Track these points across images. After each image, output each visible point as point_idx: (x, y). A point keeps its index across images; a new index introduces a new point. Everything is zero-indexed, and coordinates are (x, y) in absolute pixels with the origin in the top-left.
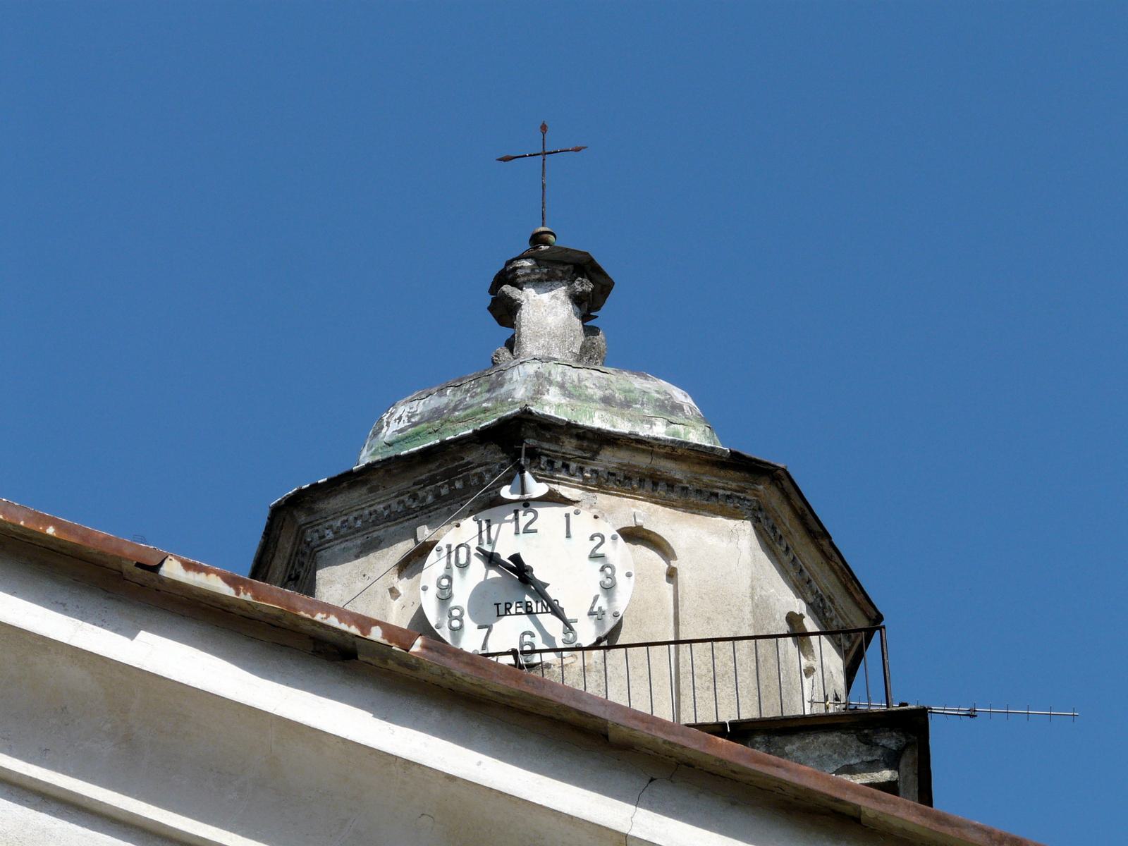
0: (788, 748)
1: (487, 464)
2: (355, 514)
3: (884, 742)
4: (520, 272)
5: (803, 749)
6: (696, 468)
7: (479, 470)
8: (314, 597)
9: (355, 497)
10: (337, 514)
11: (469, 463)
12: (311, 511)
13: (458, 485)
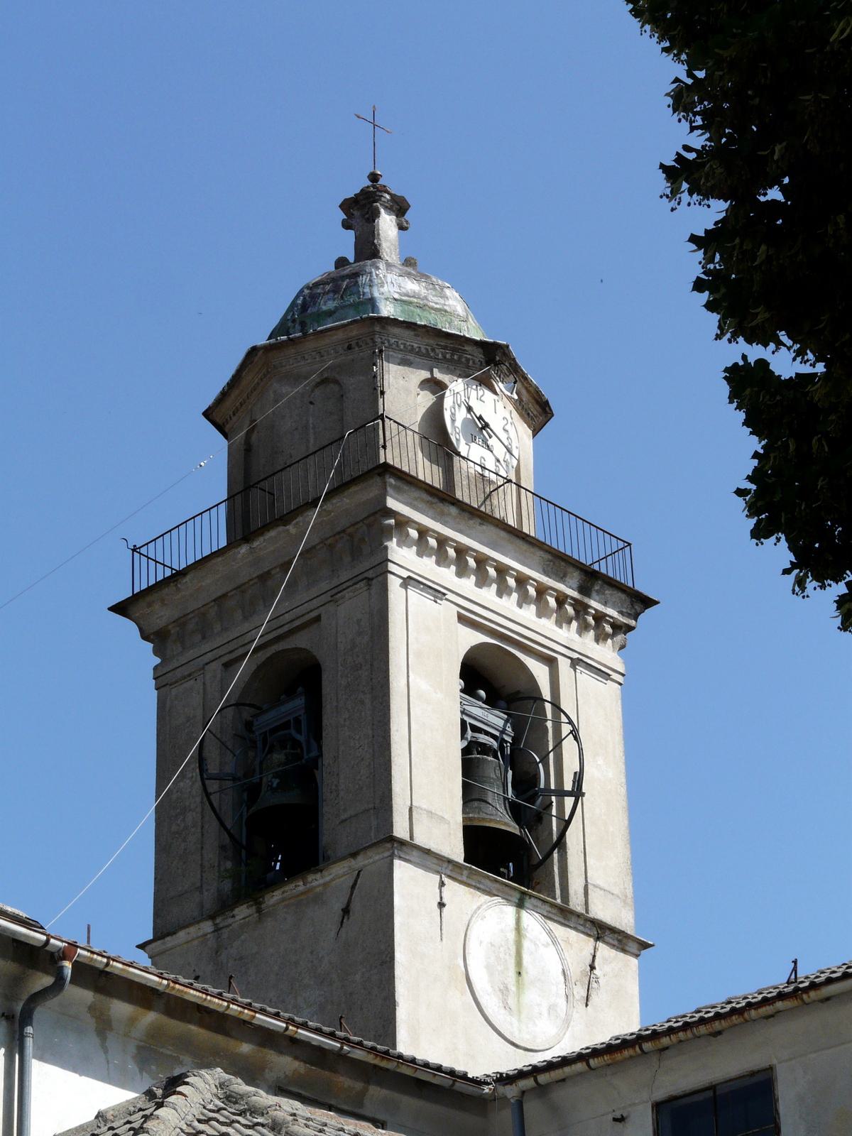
0: (607, 592)
1: (473, 356)
2: (403, 341)
3: (636, 607)
4: (383, 199)
5: (611, 595)
6: (530, 398)
7: (469, 356)
8: (845, 583)
9: (407, 333)
10: (395, 336)
11: (465, 350)
12: (383, 328)
13: (456, 357)
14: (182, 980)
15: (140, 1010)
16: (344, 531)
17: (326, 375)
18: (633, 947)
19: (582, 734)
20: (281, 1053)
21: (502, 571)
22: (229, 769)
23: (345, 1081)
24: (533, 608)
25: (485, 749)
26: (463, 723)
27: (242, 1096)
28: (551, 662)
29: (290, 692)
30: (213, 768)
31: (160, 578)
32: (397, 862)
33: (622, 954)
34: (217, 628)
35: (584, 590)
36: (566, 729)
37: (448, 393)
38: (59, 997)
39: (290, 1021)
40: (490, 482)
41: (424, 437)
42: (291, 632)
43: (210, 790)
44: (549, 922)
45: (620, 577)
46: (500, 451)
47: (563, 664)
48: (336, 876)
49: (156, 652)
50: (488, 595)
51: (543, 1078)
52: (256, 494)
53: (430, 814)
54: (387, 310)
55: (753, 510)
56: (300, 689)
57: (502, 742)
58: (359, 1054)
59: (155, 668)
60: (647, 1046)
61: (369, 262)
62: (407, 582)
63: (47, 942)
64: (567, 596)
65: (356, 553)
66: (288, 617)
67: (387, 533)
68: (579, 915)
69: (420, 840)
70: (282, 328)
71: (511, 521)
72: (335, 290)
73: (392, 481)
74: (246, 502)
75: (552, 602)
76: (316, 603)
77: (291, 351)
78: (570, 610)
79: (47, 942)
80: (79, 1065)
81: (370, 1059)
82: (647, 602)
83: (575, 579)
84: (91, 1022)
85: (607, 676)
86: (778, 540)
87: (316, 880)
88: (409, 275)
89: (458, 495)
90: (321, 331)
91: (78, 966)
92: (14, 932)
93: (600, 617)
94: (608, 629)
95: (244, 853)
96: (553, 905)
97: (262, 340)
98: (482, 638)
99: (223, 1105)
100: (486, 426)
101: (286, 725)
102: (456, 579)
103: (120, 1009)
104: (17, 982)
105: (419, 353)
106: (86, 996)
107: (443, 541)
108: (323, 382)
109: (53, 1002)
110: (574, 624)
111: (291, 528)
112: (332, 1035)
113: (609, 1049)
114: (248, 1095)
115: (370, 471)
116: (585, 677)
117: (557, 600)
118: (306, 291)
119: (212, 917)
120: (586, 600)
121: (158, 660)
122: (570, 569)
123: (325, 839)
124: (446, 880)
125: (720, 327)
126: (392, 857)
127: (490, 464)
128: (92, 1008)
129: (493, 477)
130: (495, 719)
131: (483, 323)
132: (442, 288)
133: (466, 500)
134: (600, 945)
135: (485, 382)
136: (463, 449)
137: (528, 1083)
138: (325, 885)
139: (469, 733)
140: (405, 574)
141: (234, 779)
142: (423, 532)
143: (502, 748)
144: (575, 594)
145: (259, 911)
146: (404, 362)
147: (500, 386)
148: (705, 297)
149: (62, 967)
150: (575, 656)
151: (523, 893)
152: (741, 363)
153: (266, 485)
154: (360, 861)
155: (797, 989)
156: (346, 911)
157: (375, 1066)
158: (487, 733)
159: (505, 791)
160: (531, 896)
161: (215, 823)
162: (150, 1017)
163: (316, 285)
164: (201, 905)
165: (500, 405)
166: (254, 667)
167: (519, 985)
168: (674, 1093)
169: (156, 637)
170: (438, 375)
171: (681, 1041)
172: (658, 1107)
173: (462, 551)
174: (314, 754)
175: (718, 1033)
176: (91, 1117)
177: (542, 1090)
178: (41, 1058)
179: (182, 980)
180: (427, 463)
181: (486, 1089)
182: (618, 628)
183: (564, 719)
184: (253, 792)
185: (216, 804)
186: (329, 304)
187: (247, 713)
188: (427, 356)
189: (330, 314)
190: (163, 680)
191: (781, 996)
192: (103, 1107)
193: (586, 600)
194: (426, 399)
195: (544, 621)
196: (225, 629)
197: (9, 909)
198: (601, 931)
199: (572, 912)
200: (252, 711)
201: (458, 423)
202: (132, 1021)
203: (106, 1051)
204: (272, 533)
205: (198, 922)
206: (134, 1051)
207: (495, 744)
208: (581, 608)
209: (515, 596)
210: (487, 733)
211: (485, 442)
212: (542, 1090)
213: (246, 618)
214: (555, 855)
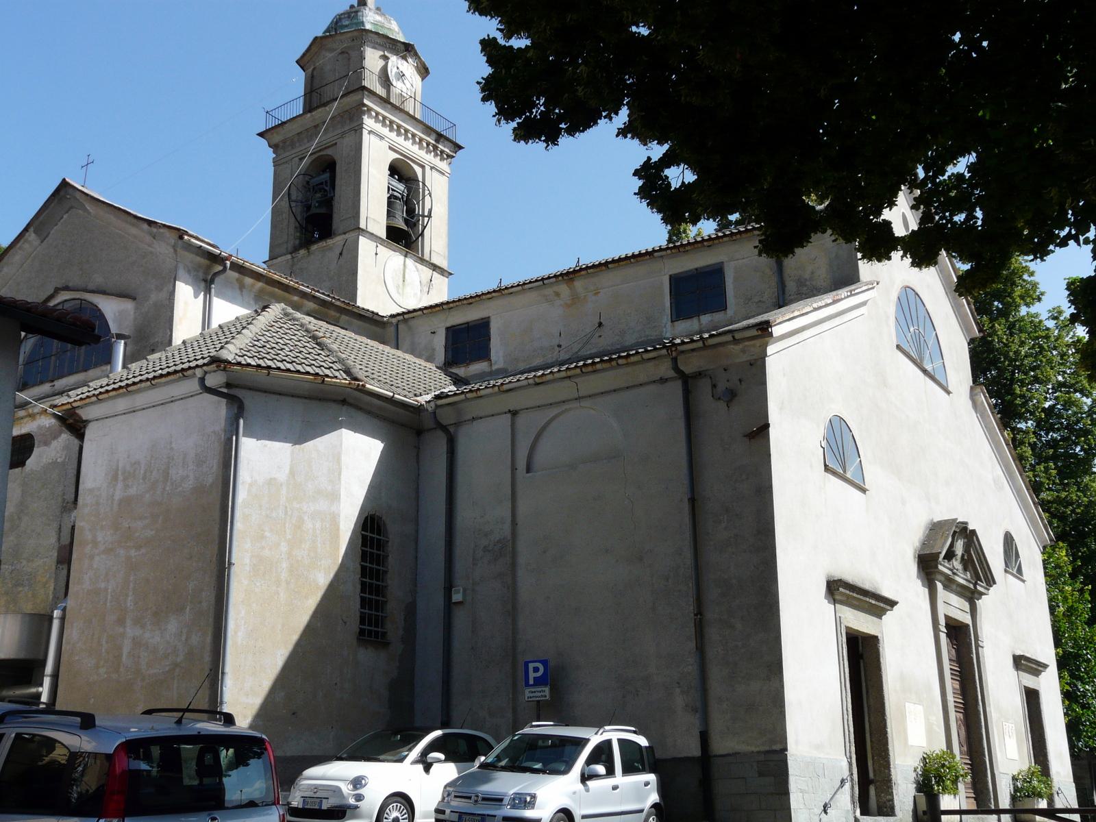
10: (370, 37)
14: (272, 271)
15: (255, 281)
16: (347, 111)
17: (343, 50)
18: (446, 274)
20: (309, 301)
21: (407, 131)
22: (299, 198)
23: (332, 313)
24: (417, 146)
25: (396, 198)
26: (389, 187)
27: (290, 314)
28: (423, 167)
29: (324, 171)
30: (294, 197)
31: (276, 124)
32: (360, 237)
33: (442, 277)
34: (297, 145)
35: (437, 141)
36: (427, 192)
37: (390, 61)
38: (224, 275)
39: (313, 289)
40: (404, 97)
41: (380, 77)
42: (326, 148)
43: (292, 206)
44: (416, 263)
45: (451, 137)
46: (409, 85)
47: (427, 168)
48: (337, 241)
49: (274, 152)
50: (401, 140)
51: (406, 316)
52: (314, 94)
53: (374, 220)
54: (368, 27)
55: (483, 90)
57: (403, 196)
58: (338, 303)
59: (274, 158)
60: (444, 307)
61: (362, 7)
62: (370, 132)
63: (393, 396)
64: (430, 143)
65: (351, 119)
66: (325, 142)
67: (363, 113)
68: (427, 261)
69: (369, 230)
70: (328, 30)
71: (411, 113)
72: (349, 17)
73: (366, 93)
74: (311, 96)
75: (425, 144)
76: (335, 138)
77: (331, 39)
78: (431, 148)
79: (393, 396)
80: (232, 300)
81: (342, 305)
82: (460, 148)
83: (434, 136)
84: (237, 285)
85: (443, 174)
86: (491, 103)
87: (330, 242)
88: (377, 14)
89: (391, 101)
90: (343, 33)
91: (232, 263)
92: (207, 249)
93: (442, 152)
94: (445, 156)
95: (304, 230)
96: (418, 257)
97: (320, 34)
98: (398, 156)
99: (300, 328)
100: (404, 75)
101: (322, 184)
102: (389, 133)
103: (248, 281)
104: (209, 268)
105: (380, 45)
106: (235, 275)
107: (385, 118)
108: (342, 53)
109: (222, 277)
110: (433, 153)
111: (327, 108)
112: (328, 296)
113: (431, 307)
114: (292, 313)
115: (358, 89)
116: (435, 173)
117: (427, 144)
118: (338, 17)
119: (291, 253)
120: (437, 145)
121: (274, 156)
122: (433, 133)
123: (334, 227)
124: (378, 245)
125: (469, 8)
126: (359, 235)
127: (404, 90)
128: (237, 280)
129: (405, 95)
130: (401, 187)
131: (404, 34)
132: (390, 20)
133: (394, 103)
134: (434, 272)
135: (404, 58)
136: (394, 83)
137: (401, 317)
138: (333, 244)
140: (369, 129)
141: (302, 202)
142: (377, 114)
143: (403, 198)
144: (433, 142)
145: (308, 252)
146: (374, 48)
147: (410, 60)
149: (226, 263)
150: (432, 165)
151: (407, 252)
152: (487, 38)
153: (318, 91)
154: (347, 236)
155: (500, 289)
156: (341, 254)
157: (344, 308)
158: (397, 192)
159: (403, 214)
160: (410, 253)
161: (294, 219)
162: (260, 285)
163: (342, 14)
164: (287, 248)
165: (410, 67)
166: (310, 161)
167: (404, 285)
168: (454, 324)
169: (275, 147)
170: (386, 54)
171: (529, 384)
172: (448, 329)
173: (391, 122)
174: (332, 195)
175: (471, 303)
176: (233, 318)
177: (405, 321)
178: (217, 296)
179: (272, 271)
180: (380, 88)
181: (385, 319)
182: (449, 156)
183: (426, 188)
184: (308, 208)
185: (294, 211)
186: (346, 22)
187: (307, 178)
188: (383, 46)
189: (346, 26)
190: (276, 163)
191: (494, 291)
192: (238, 315)
193: (437, 145)
194: (381, 63)
195: (421, 151)
196: (300, 145)
197: (206, 240)
198: (435, 267)
199: (424, 260)
200: (310, 177)
201: (393, 73)
202: (253, 285)
203: (242, 295)
204: (320, 110)
205: (285, 255)
206: (253, 296)
207: (400, 196)
208: (435, 148)
209: (411, 141)
210: (397, 192)
211: (403, 81)
212: (405, 321)
213: (308, 142)
214: (420, 239)
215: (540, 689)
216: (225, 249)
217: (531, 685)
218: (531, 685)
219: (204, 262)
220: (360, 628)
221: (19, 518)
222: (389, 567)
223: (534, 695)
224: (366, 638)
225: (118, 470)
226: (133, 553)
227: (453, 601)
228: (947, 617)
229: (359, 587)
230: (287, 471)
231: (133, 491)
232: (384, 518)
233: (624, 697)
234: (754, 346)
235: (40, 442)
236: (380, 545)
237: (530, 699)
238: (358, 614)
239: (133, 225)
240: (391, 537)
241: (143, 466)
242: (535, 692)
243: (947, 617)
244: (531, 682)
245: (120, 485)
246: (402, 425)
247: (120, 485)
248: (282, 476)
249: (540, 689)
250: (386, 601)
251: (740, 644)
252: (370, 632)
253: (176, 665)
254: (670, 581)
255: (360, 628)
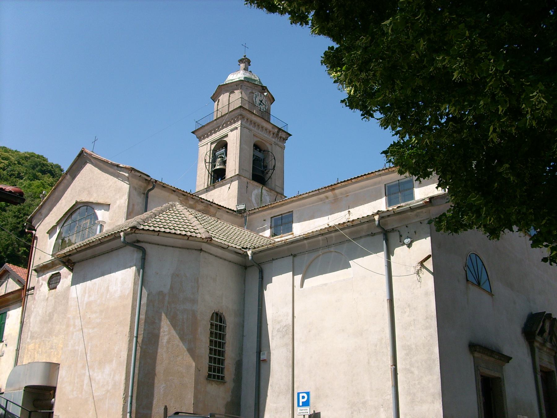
19: (276, 159)
56: (224, 147)
101: (221, 154)
139: (255, 157)
148: (393, 144)
174: (226, 159)
215: (305, 408)
216: (154, 176)
217: (301, 406)
218: (301, 406)
219: (144, 184)
220: (209, 374)
221: (53, 315)
222: (227, 340)
223: (302, 411)
224: (220, 380)
225: (86, 287)
226: (91, 331)
227: (261, 359)
228: (540, 366)
229: (208, 351)
230: (169, 287)
231: (92, 298)
232: (224, 314)
233: (352, 413)
234: (422, 212)
235: (63, 276)
236: (222, 328)
237: (300, 414)
238: (208, 366)
239: (111, 168)
240: (227, 323)
241: (97, 285)
242: (302, 410)
243: (540, 366)
244: (301, 404)
245: (87, 295)
246: (233, 262)
247: (87, 295)
248: (166, 290)
249: (305, 408)
250: (224, 359)
251: (417, 382)
252: (214, 376)
253: (108, 391)
254: (377, 346)
255: (209, 374)
